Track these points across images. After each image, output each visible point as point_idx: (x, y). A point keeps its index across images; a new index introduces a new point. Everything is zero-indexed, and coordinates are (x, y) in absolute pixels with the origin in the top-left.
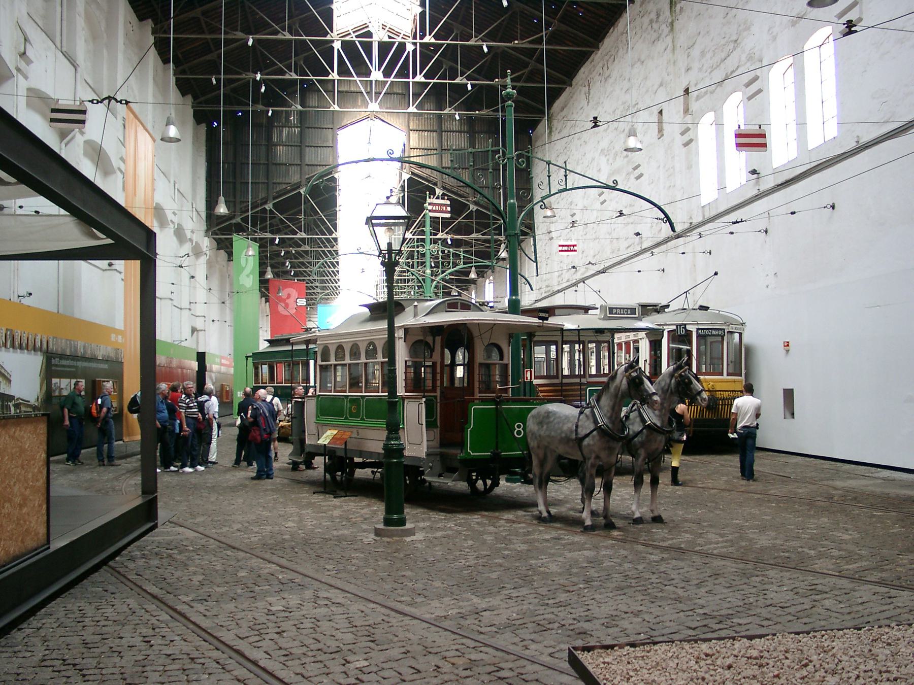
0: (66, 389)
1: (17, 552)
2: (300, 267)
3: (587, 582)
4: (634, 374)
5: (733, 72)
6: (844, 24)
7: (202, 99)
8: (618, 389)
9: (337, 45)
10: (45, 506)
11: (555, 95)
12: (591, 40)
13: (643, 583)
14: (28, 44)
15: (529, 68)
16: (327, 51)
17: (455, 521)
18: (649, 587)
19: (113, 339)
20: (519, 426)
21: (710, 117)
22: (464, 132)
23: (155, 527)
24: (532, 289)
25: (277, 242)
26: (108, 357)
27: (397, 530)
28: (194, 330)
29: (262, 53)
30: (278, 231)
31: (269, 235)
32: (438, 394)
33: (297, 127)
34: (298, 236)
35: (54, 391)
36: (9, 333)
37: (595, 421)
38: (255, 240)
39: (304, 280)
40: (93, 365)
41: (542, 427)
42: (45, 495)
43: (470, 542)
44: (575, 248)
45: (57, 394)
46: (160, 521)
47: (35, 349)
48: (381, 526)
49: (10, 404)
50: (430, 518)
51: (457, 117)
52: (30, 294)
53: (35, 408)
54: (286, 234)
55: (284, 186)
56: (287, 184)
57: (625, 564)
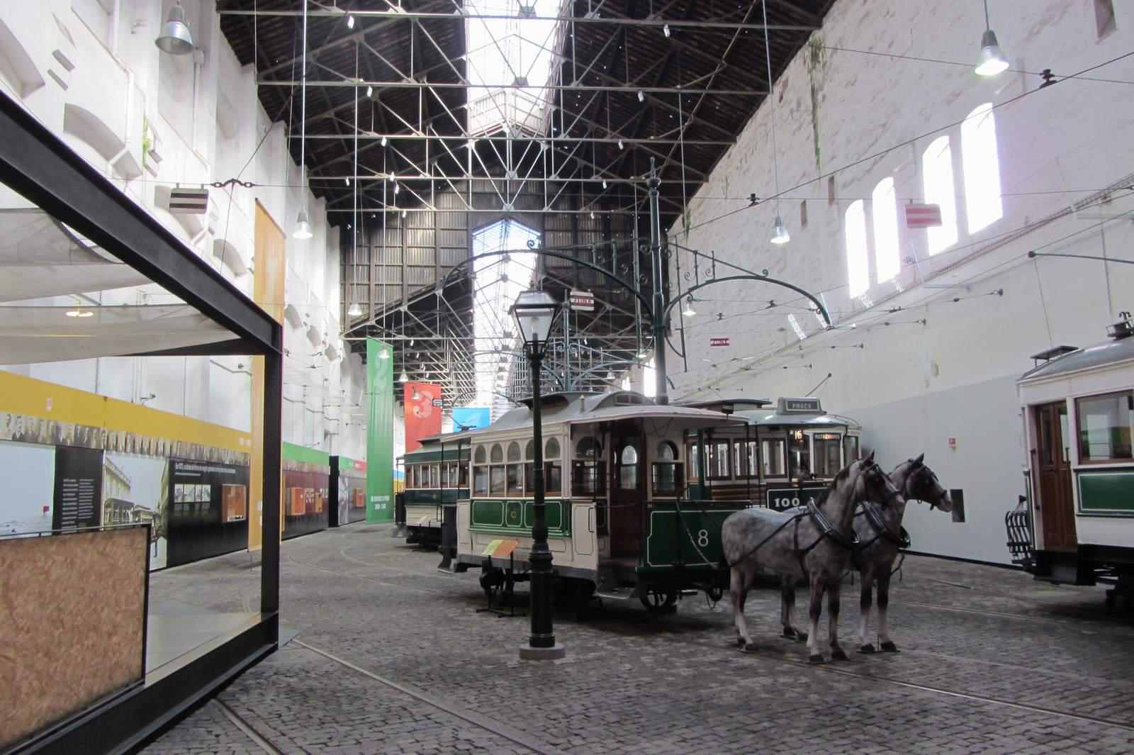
0: (190, 495)
1: (102, 691)
2: (435, 370)
3: (771, 719)
4: (872, 472)
5: (876, 163)
6: (1041, 74)
7: (336, 201)
8: (851, 489)
9: (471, 145)
10: (140, 634)
11: (692, 190)
12: (728, 133)
13: (838, 721)
14: (157, 141)
15: (665, 164)
16: (462, 155)
17: (607, 639)
18: (847, 726)
19: (242, 443)
20: (703, 534)
21: (858, 205)
22: (600, 231)
23: (275, 648)
24: (673, 388)
25: (412, 344)
26: (236, 461)
27: (545, 651)
28: (326, 434)
29: (384, 108)
30: (413, 335)
31: (403, 337)
32: (608, 496)
33: (431, 229)
34: (434, 338)
35: (177, 497)
36: (129, 437)
37: (820, 528)
38: (389, 342)
39: (439, 383)
40: (220, 470)
41: (747, 535)
42: (142, 621)
43: (628, 666)
44: (728, 342)
45: (180, 500)
46: (281, 642)
47: (157, 453)
48: (527, 646)
49: (129, 512)
50: (579, 635)
51: (592, 216)
52: (154, 396)
53: (155, 516)
54: (421, 336)
55: (419, 288)
56: (422, 285)
57: (811, 696)
